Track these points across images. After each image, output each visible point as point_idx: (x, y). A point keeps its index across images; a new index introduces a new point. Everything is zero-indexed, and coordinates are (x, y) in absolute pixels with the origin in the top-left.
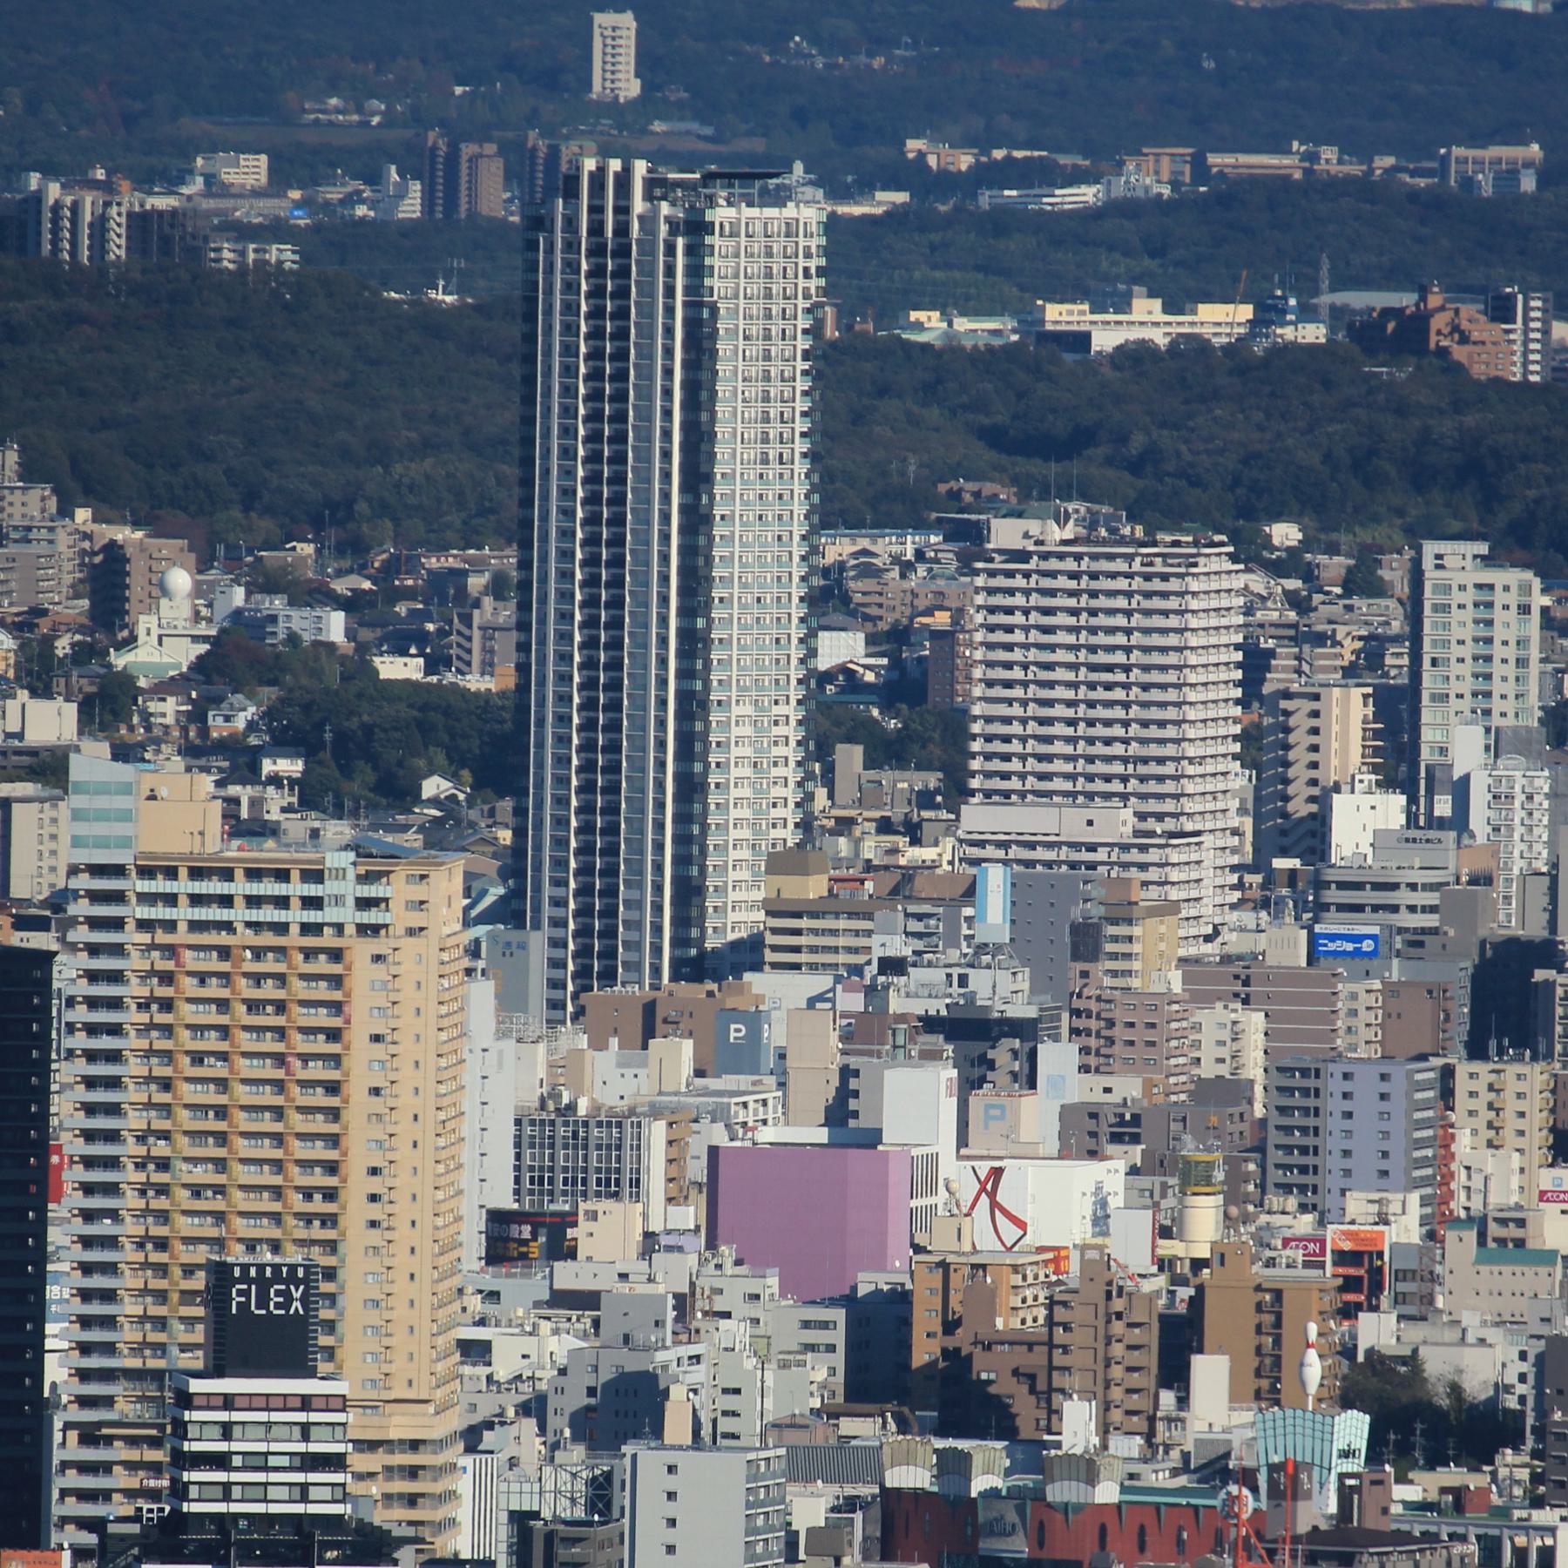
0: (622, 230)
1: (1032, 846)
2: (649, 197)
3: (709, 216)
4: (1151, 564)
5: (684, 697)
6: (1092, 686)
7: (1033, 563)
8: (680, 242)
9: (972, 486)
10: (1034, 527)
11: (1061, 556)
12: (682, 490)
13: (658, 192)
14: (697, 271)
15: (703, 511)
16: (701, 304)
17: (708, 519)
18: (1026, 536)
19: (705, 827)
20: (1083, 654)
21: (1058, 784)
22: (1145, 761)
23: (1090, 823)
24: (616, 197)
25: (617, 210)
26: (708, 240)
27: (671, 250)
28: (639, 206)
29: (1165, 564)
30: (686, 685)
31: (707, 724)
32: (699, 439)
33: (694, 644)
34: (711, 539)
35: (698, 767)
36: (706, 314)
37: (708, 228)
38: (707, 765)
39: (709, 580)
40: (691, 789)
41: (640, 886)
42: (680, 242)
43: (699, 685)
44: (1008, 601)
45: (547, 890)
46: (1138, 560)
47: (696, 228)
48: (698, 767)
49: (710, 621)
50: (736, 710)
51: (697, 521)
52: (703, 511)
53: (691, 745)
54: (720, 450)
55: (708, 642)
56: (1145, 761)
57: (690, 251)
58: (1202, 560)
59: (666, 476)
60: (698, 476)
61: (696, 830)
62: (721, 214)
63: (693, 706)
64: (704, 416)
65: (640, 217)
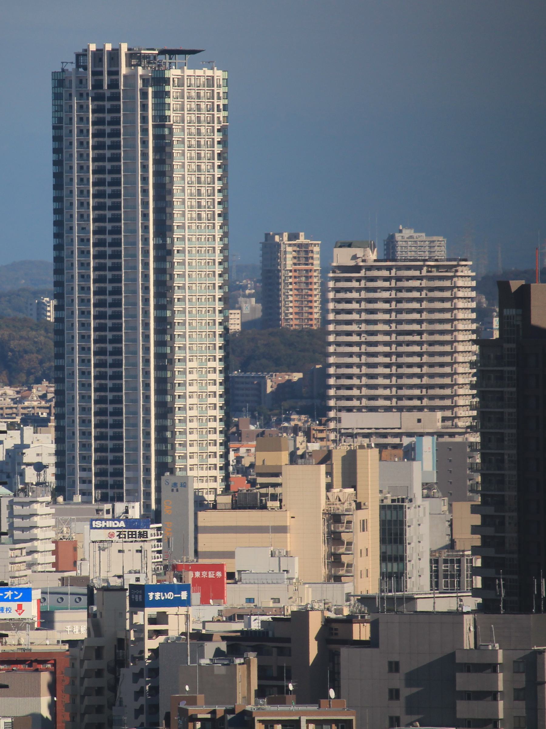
0: (114, 85)
1: (385, 436)
2: (129, 65)
3: (167, 74)
4: (431, 272)
5: (159, 356)
6: (399, 344)
7: (362, 273)
8: (150, 90)
9: (138, 530)
10: (359, 252)
11: (379, 268)
12: (156, 235)
13: (134, 62)
14: (161, 106)
15: (168, 248)
16: (164, 126)
17: (170, 253)
18: (354, 257)
19: (173, 433)
20: (393, 325)
21: (381, 402)
22: (432, 387)
23: (419, 421)
24: (110, 65)
25: (110, 73)
26: (167, 88)
27: (144, 95)
28: (124, 70)
29: (438, 271)
30: (161, 350)
31: (173, 372)
32: (164, 193)
33: (164, 325)
34: (172, 264)
35: (169, 398)
36: (167, 131)
37: (166, 81)
38: (174, 397)
39: (172, 288)
40: (165, 411)
41: (137, 470)
42: (150, 90)
43: (168, 350)
44: (349, 295)
45: (78, 474)
46: (425, 269)
47: (159, 81)
48: (169, 398)
49: (173, 312)
50: (189, 365)
51: (164, 253)
52: (168, 248)
53: (164, 386)
54: (176, 212)
55: (172, 324)
56: (432, 387)
57: (156, 95)
58: (460, 269)
59: (146, 228)
60: (164, 228)
61: (169, 434)
62: (173, 73)
63: (165, 362)
64: (169, 240)
65: (125, 76)
